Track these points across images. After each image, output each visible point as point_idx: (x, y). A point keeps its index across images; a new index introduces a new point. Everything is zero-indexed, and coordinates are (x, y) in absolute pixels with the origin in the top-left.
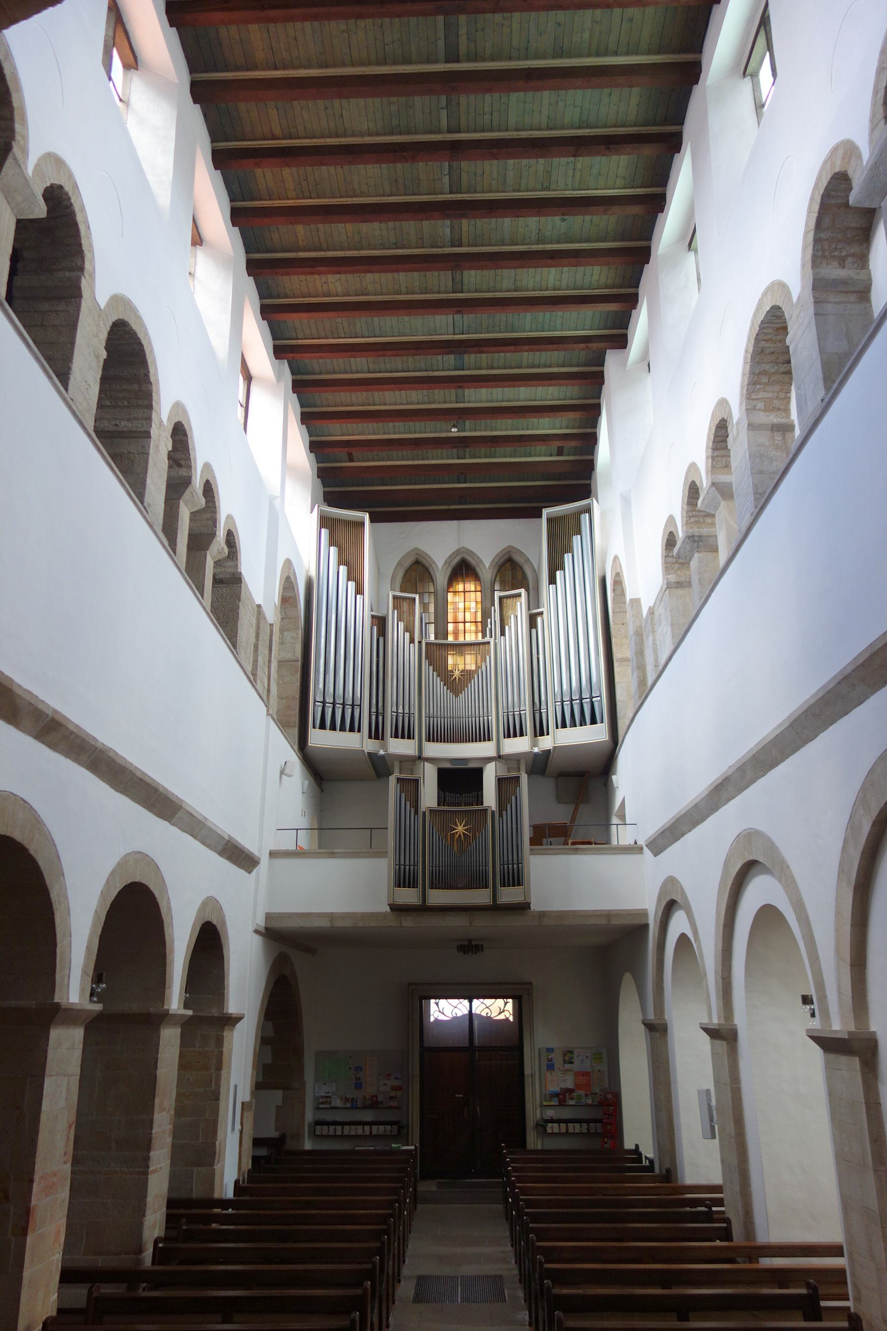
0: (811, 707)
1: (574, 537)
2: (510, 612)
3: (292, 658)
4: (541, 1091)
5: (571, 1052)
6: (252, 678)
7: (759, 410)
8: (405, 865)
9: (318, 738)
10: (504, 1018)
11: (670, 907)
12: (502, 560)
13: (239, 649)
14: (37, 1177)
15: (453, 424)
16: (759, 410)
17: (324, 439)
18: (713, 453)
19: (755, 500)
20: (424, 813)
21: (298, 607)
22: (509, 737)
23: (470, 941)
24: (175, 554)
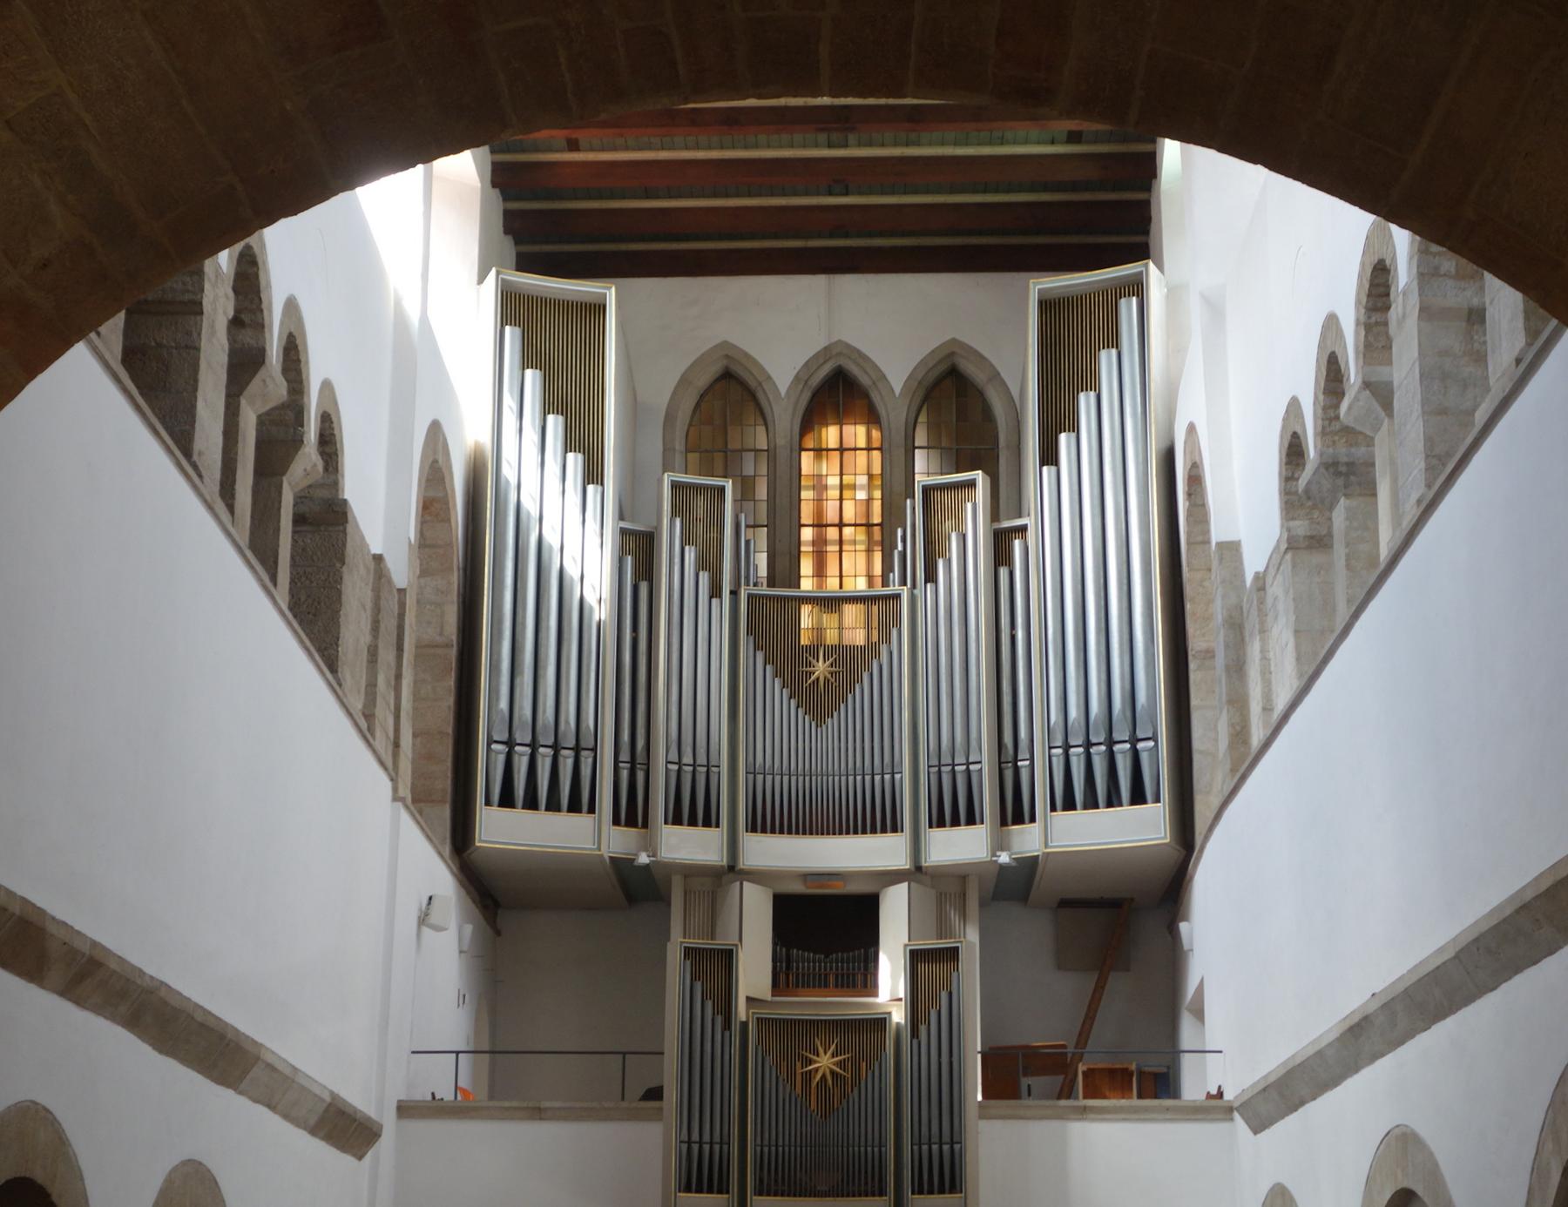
1: (1103, 354)
2: (948, 524)
3: (439, 639)
6: (366, 724)
7: (1445, 275)
8: (701, 1143)
16: (1445, 275)
18: (1369, 317)
19: (1426, 470)
20: (744, 1025)
21: (453, 521)
22: (941, 824)
24: (275, 585)
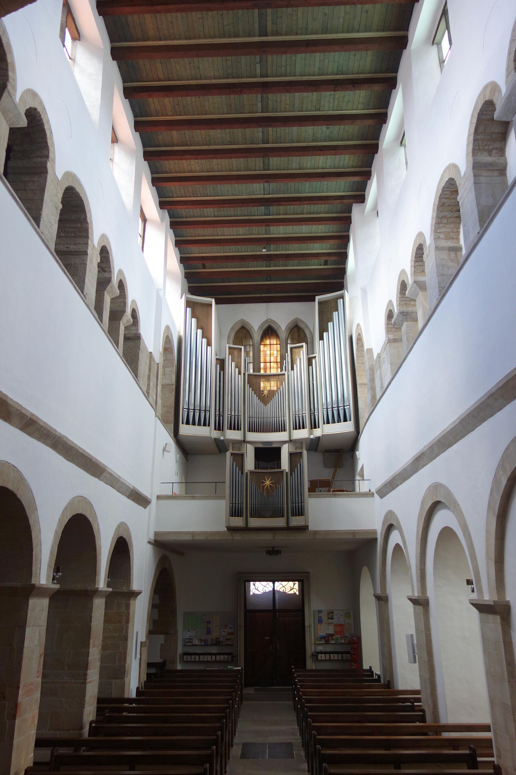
0: (472, 411)
1: (334, 313)
2: (297, 356)
3: (170, 383)
4: (315, 635)
5: (332, 613)
6: (147, 395)
7: (441, 239)
8: (235, 504)
9: (185, 430)
10: (293, 593)
11: (389, 528)
12: (292, 326)
13: (139, 378)
14: (21, 686)
15: (263, 247)
16: (441, 239)
17: (188, 255)
18: (415, 264)
19: (439, 291)
20: (247, 473)
21: (174, 353)
22: (296, 429)
23: (273, 548)
